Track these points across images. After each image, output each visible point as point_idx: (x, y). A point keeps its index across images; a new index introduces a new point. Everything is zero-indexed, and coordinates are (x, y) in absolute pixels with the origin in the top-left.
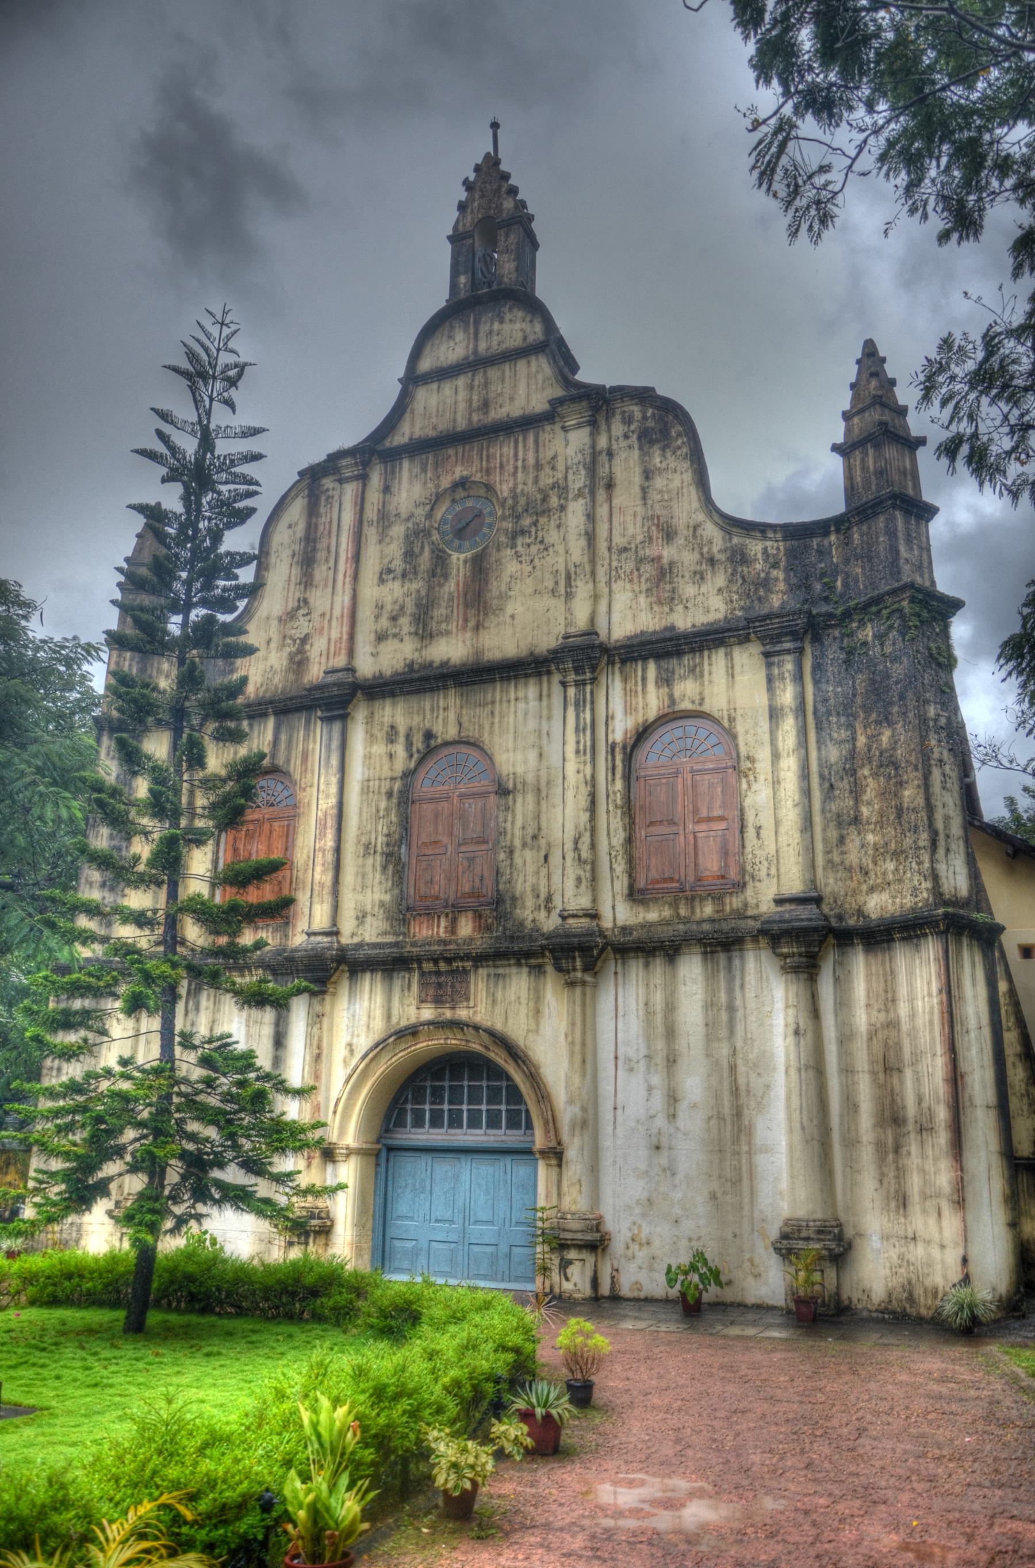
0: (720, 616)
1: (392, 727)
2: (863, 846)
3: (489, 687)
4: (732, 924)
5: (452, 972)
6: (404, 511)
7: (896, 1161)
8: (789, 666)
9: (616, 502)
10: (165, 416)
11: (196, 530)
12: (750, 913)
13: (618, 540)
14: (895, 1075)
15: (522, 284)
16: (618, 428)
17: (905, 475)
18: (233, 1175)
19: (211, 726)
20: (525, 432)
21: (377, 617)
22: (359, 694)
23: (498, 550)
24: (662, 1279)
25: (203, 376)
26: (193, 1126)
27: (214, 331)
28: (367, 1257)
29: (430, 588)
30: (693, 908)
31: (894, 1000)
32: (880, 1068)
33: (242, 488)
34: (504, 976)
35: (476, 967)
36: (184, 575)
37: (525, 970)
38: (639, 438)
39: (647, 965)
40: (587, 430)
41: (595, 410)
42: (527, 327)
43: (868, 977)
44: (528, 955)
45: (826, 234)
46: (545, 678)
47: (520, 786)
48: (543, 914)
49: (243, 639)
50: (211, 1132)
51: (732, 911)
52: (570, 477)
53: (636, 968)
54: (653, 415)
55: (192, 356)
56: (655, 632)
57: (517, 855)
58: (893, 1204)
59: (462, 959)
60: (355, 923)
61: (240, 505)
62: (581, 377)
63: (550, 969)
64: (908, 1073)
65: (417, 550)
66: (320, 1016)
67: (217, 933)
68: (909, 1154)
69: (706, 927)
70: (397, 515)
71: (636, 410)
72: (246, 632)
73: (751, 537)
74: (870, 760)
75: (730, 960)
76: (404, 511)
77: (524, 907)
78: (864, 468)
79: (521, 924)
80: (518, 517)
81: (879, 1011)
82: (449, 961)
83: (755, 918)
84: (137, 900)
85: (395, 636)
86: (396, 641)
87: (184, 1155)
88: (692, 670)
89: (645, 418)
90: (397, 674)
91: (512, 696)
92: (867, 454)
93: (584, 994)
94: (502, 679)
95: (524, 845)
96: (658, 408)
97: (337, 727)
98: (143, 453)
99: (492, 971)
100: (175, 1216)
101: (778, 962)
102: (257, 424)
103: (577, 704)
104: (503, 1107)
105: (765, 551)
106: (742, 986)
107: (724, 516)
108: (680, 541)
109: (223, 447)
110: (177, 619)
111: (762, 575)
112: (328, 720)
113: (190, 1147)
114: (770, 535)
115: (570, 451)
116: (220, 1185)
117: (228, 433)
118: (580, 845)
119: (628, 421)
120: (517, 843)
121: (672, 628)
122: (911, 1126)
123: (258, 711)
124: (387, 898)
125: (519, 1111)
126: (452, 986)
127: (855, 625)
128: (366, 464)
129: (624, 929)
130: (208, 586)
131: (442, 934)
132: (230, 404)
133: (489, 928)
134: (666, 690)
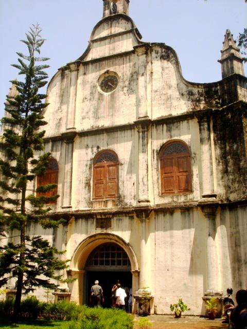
0: (185, 111)
1: (87, 145)
2: (229, 179)
3: (116, 133)
4: (190, 203)
5: (106, 219)
6: (90, 81)
7: (238, 272)
8: (206, 126)
9: (153, 77)
10: (21, 55)
11: (30, 88)
12: (195, 200)
13: (154, 88)
14: (238, 247)
15: (125, 13)
16: (154, 54)
17: (239, 69)
18: (42, 277)
19: (33, 146)
20: (126, 56)
21: (82, 112)
22: (77, 136)
23: (119, 92)
24: (169, 309)
25: (32, 43)
26: (30, 263)
27: (35, 30)
28: (96, 129)
29: (98, 104)
30: (178, 198)
31: (238, 225)
32: (234, 245)
33: (43, 76)
34: (121, 219)
35: (113, 217)
36: (26, 101)
38: (160, 58)
39: (164, 216)
40: (145, 55)
41: (147, 50)
42: (126, 25)
43: (230, 218)
45: (110, 117)
46: (133, 130)
49: (43, 120)
50: (36, 265)
51: (190, 199)
52: (140, 70)
53: (161, 217)
54: (164, 51)
55: (29, 38)
56: (166, 116)
57: (125, 183)
58: (238, 285)
61: (42, 81)
62: (142, 40)
63: (135, 217)
64: (242, 246)
65: (94, 92)
66: (66, 232)
67: (35, 206)
68: (242, 270)
69: (182, 204)
70: (88, 82)
71: (159, 49)
72: (43, 118)
73: (195, 87)
74: (230, 154)
75: (189, 214)
76: (90, 81)
77: (127, 199)
78: (227, 66)
79: (126, 204)
80: (124, 82)
81: (234, 228)
82: (105, 215)
83: (196, 201)
84: (12, 196)
85: (88, 118)
86: (88, 119)
87: (27, 272)
88: (177, 127)
89: (162, 52)
91: (123, 136)
92: (228, 63)
93: (145, 224)
94: (120, 131)
95: (127, 181)
96: (166, 49)
97: (70, 145)
98: (14, 66)
99: (118, 218)
100: (26, 289)
101: (203, 214)
102: (47, 57)
103: (143, 138)
104: (122, 259)
105: (198, 91)
106: (193, 222)
107: (186, 81)
108: (173, 88)
109: (36, 64)
110: (24, 114)
111: (198, 99)
112: (68, 143)
113: (29, 269)
114: (200, 86)
115: (140, 62)
116: (38, 280)
117: (38, 59)
118: (144, 180)
119: (157, 53)
120: (125, 179)
121: (171, 115)
122: (243, 262)
123: (47, 141)
125: (126, 260)
126: (106, 222)
127: (225, 113)
128: (78, 66)
129: (157, 205)
130: (33, 104)
132: (39, 51)
133: (117, 205)
134: (169, 133)
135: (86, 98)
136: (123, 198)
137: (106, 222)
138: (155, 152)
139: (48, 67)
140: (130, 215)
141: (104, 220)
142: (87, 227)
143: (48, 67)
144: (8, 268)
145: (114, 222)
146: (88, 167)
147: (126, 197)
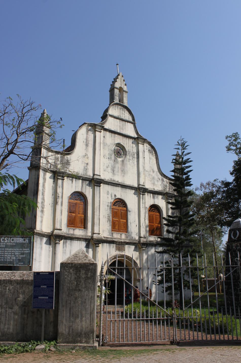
57: (132, 224)
85: (108, 171)
95: (133, 222)
99: (128, 246)
102: (189, 158)
120: (132, 222)
136: (130, 233)
141: (120, 245)
142: (110, 249)
144: (176, 179)
147: (132, 233)
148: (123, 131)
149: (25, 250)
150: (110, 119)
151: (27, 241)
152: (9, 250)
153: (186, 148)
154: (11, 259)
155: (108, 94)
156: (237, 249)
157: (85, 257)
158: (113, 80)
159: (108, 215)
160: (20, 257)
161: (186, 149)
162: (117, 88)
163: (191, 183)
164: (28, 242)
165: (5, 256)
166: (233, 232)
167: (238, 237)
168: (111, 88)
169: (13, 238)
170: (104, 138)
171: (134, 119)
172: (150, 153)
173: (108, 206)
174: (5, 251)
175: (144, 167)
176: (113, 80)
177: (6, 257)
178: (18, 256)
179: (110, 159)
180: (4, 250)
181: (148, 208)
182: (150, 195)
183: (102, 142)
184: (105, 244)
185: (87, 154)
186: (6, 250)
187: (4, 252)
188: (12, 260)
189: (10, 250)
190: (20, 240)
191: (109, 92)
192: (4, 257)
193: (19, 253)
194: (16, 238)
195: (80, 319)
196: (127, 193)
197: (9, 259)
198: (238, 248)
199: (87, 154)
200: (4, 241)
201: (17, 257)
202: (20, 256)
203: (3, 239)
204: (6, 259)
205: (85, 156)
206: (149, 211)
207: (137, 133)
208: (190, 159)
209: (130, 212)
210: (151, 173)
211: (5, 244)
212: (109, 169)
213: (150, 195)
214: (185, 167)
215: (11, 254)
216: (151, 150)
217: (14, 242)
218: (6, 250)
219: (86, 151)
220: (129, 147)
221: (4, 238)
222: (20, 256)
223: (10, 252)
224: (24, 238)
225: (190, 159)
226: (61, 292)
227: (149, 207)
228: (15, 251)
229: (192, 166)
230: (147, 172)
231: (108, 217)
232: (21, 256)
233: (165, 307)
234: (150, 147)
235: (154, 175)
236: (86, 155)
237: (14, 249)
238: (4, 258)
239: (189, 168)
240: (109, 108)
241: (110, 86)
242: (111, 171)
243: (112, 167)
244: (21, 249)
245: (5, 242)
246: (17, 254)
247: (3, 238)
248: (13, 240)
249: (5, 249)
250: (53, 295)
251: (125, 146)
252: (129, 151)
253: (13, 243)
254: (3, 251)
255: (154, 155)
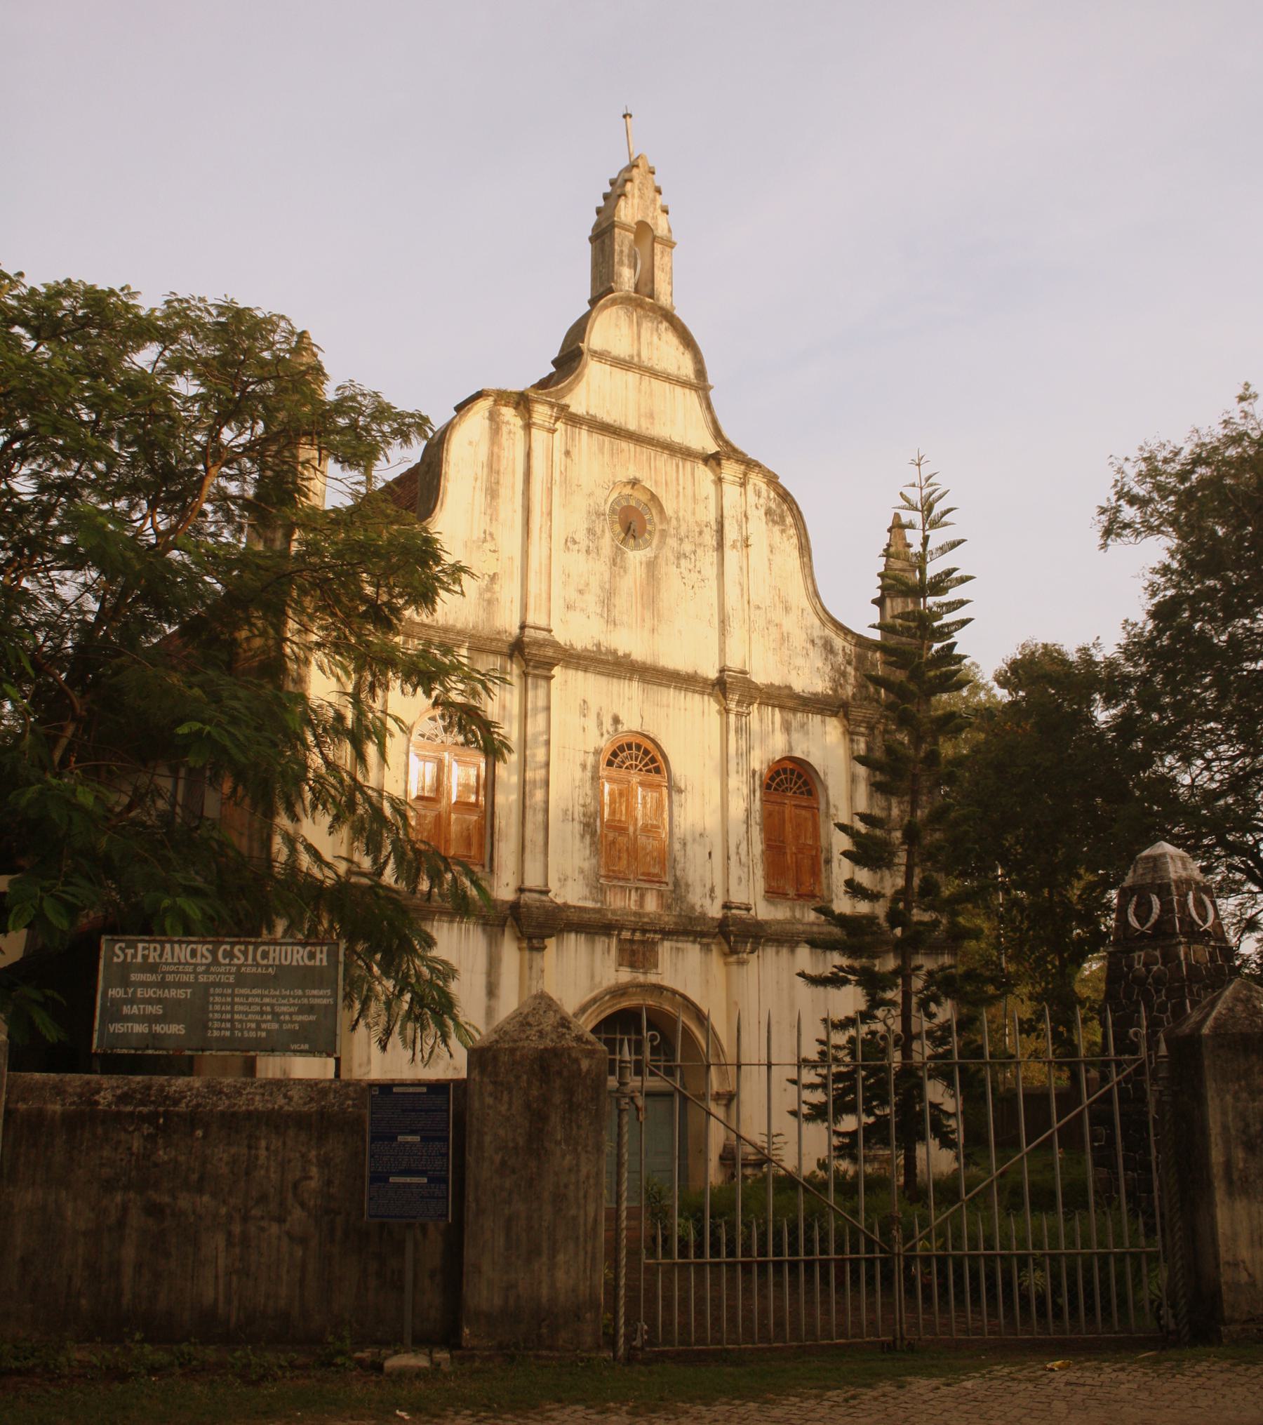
3: (664, 690)
5: (643, 942)
34: (682, 950)
35: (662, 939)
37: (697, 947)
44: (703, 935)
47: (689, 788)
48: (707, 902)
57: (689, 847)
59: (655, 932)
60: (558, 884)
65: (599, 532)
79: (693, 907)
82: (644, 931)
85: (582, 610)
90: (586, 650)
94: (675, 687)
95: (694, 840)
99: (674, 944)
114: (849, 638)
124: (586, 865)
126: (644, 954)
131: (633, 907)
135: (575, 542)
137: (644, 954)
138: (757, 777)
139: (969, 620)
140: (705, 940)
142: (592, 961)
143: (969, 620)
145: (665, 949)
146: (589, 774)
147: (691, 889)
148: (652, 424)
149: (314, 996)
150: (593, 371)
151: (321, 960)
152: (254, 996)
153: (944, 519)
154: (258, 1028)
155: (584, 253)
156: (1149, 971)
157: (563, 1026)
158: (608, 189)
159: (584, 806)
160: (295, 1022)
161: (946, 524)
162: (625, 227)
163: (957, 651)
164: (325, 963)
165: (237, 1017)
166: (1135, 899)
167: (1157, 922)
168: (597, 225)
169: (266, 948)
170: (569, 461)
171: (701, 372)
172: (774, 522)
173: (584, 767)
174: (236, 1000)
175: (744, 589)
176: (608, 189)
177: (241, 1021)
178: (287, 1018)
179: (593, 555)
180: (233, 995)
181: (761, 776)
182: (773, 715)
183: (557, 475)
184: (573, 936)
185: (491, 535)
186: (240, 996)
187: (233, 1004)
188: (264, 1034)
189: (257, 996)
190: (295, 956)
191: (589, 246)
192: (232, 1021)
193: (294, 1005)
194: (278, 948)
195: (544, 1259)
196: (668, 706)
197: (250, 1029)
198: (1155, 968)
199: (493, 530)
200: (231, 959)
201: (284, 1022)
202: (295, 1018)
203: (225, 950)
204: (241, 1030)
205: (485, 541)
206: (768, 787)
207: (718, 434)
208: (955, 570)
209: (680, 791)
210: (777, 616)
211: (234, 969)
212: (591, 601)
213: (773, 715)
214: (940, 606)
215: (258, 1008)
216: (778, 511)
217: (271, 962)
218: (240, 996)
219: (488, 518)
220: (678, 496)
221: (232, 948)
222: (295, 1018)
223: (257, 1004)
224: (308, 948)
225: (955, 570)
226: (470, 1159)
227: (765, 771)
228: (273, 997)
229: (968, 602)
230: (758, 612)
231: (584, 815)
232: (300, 1018)
233: (1061, 1209)
234: (772, 494)
235: (790, 624)
236: (488, 536)
237: (273, 992)
238: (233, 1025)
239: (955, 609)
240: (590, 321)
241: (594, 218)
242: (599, 611)
243: (602, 588)
244: (300, 992)
245: (236, 961)
246: (284, 1009)
247: (228, 947)
248: (265, 955)
249: (237, 991)
250: (448, 1171)
251: (659, 496)
252: (678, 519)
253: (267, 967)
254: (229, 999)
255: (792, 531)
